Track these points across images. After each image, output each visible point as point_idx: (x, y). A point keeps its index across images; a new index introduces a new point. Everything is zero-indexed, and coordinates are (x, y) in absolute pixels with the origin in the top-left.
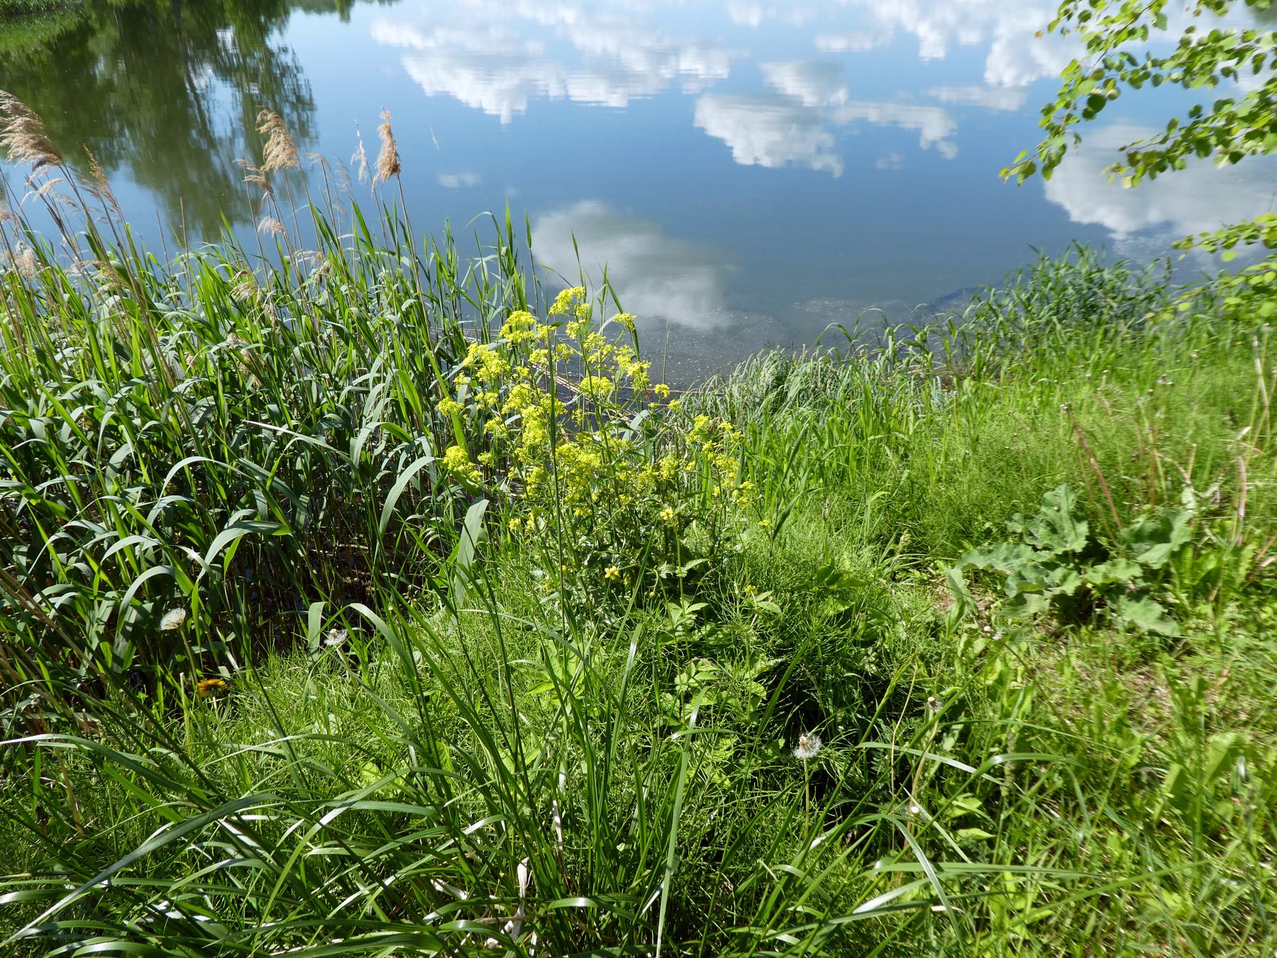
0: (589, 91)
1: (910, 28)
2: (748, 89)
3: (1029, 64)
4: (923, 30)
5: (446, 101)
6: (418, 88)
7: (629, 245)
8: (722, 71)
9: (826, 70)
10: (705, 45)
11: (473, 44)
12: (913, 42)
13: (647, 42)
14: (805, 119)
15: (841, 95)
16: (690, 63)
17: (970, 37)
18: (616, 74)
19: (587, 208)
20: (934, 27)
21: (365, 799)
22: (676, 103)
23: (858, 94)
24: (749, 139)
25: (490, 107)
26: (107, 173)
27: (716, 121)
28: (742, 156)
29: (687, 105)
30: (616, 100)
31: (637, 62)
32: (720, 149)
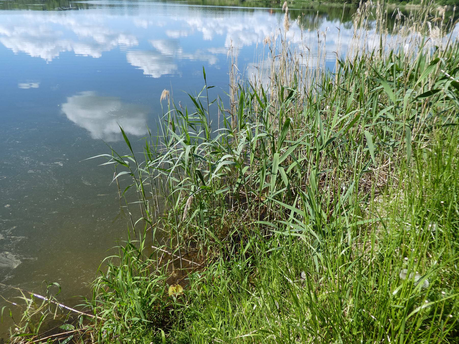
0: (83, 51)
1: (199, 29)
2: (147, 49)
3: (238, 41)
4: (204, 30)
5: (23, 55)
6: (10, 51)
7: (113, 107)
8: (135, 42)
9: (173, 43)
10: (127, 34)
11: (32, 32)
12: (201, 34)
13: (104, 32)
14: (168, 60)
15: (180, 51)
16: (123, 40)
17: (221, 32)
18: (95, 45)
19: (88, 94)
20: (207, 28)
21: (399, 328)
22: (119, 56)
23: (186, 51)
24: (150, 68)
25: (43, 56)
26: (243, 65)
27: (134, 60)
28: (146, 72)
29: (123, 57)
30: (96, 55)
31: (100, 39)
32: (139, 72)
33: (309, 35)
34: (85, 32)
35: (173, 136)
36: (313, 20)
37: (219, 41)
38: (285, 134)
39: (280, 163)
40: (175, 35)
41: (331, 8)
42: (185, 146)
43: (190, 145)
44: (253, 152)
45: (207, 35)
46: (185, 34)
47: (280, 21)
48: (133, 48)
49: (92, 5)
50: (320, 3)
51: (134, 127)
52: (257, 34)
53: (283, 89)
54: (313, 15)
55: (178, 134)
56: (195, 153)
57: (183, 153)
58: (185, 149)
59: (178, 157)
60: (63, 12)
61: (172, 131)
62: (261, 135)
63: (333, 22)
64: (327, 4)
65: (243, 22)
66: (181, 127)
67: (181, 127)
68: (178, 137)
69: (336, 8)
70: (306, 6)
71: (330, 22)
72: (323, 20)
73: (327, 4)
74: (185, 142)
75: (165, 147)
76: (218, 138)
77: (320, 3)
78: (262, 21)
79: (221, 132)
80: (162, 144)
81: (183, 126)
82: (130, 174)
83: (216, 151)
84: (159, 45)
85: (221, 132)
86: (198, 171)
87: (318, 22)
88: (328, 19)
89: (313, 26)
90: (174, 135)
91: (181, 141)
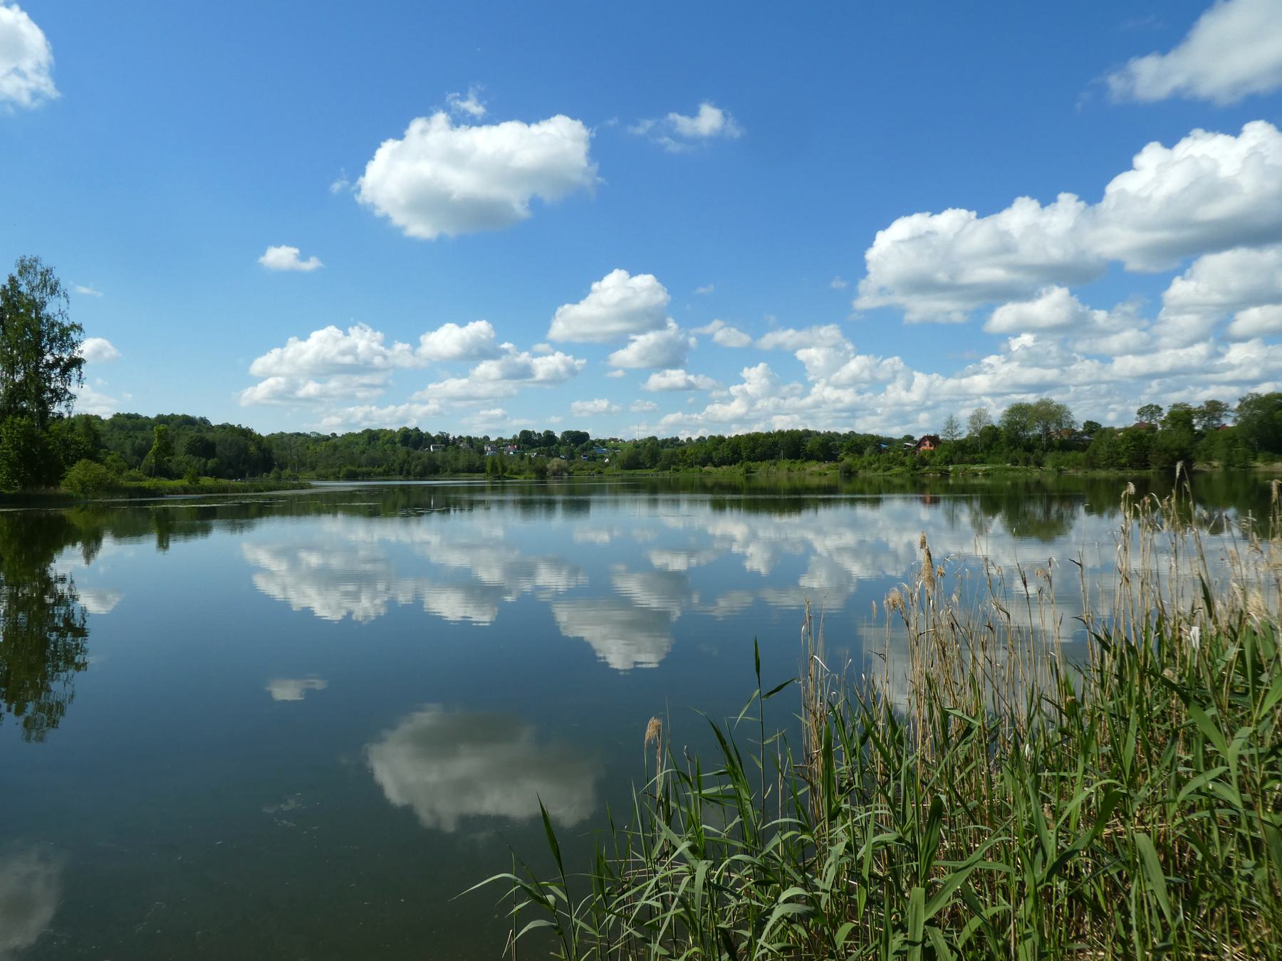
0: (448, 606)
9: (675, 583)
10: (557, 563)
16: (549, 579)
22: (536, 613)
30: (483, 617)
31: (490, 575)
33: (1032, 553)
34: (456, 559)
35: (664, 835)
36: (1047, 512)
37: (789, 567)
38: (934, 837)
39: (931, 914)
40: (678, 563)
41: (1093, 483)
42: (694, 862)
43: (705, 858)
44: (863, 883)
45: (757, 560)
46: (704, 558)
47: (953, 519)
48: (570, 596)
49: (482, 502)
50: (1060, 471)
51: (568, 806)
52: (895, 555)
53: (945, 715)
54: (1045, 501)
55: (678, 831)
56: (714, 880)
57: (686, 879)
58: (692, 871)
59: (677, 890)
60: (413, 520)
61: (662, 823)
62: (880, 837)
63: (1106, 516)
64: (1080, 474)
65: (855, 525)
66: (685, 810)
67: (685, 810)
68: (674, 838)
69: (1107, 481)
70: (1021, 481)
71: (1094, 517)
72: (1075, 514)
73: (1080, 474)
74: (693, 849)
75: (643, 865)
76: (776, 840)
77: (1060, 471)
78: (901, 521)
79: (784, 828)
80: (634, 857)
81: (690, 810)
82: (556, 928)
83: (767, 878)
84: (632, 586)
85: (784, 828)
86: (723, 930)
87: (1060, 517)
88: (1090, 510)
89: (1048, 530)
90: (666, 833)
91: (683, 847)
